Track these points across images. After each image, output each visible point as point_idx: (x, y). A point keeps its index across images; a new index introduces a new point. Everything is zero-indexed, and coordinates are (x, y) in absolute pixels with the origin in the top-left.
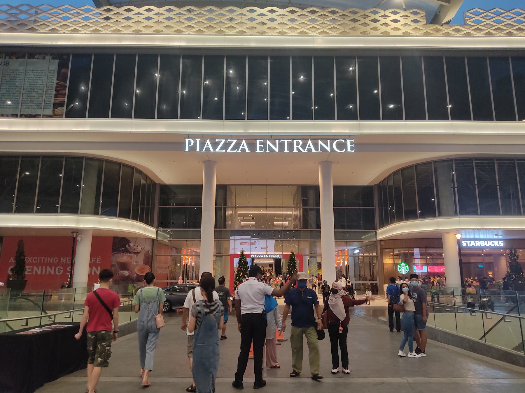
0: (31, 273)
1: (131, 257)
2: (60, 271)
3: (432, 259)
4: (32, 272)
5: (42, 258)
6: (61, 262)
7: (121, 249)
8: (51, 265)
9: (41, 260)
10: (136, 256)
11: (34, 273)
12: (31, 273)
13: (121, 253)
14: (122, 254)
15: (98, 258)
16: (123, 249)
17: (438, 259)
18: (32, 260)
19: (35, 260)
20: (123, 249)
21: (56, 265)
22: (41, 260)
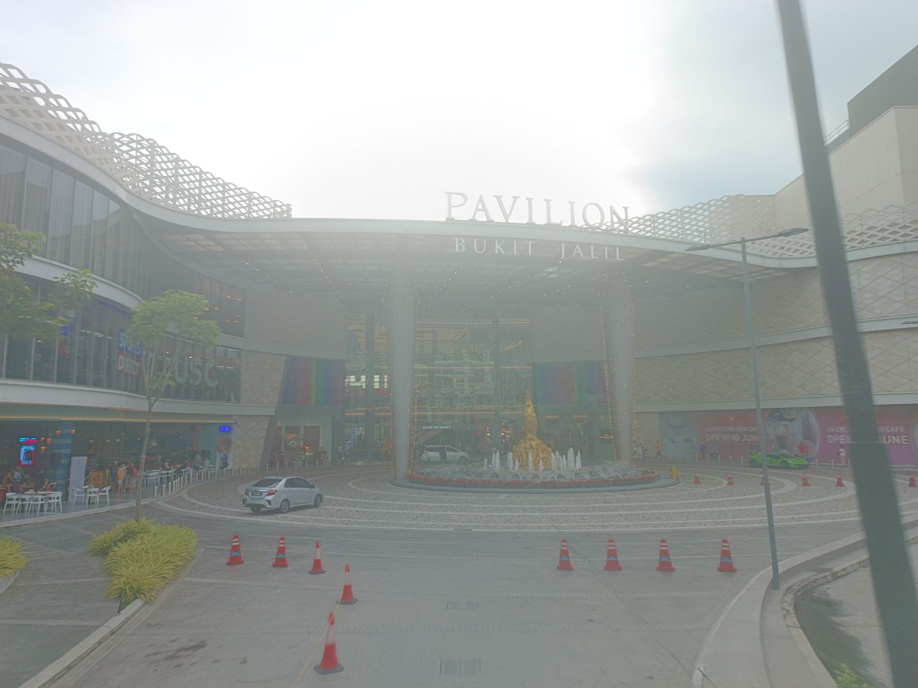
16: (778, 414)
20: (778, 414)
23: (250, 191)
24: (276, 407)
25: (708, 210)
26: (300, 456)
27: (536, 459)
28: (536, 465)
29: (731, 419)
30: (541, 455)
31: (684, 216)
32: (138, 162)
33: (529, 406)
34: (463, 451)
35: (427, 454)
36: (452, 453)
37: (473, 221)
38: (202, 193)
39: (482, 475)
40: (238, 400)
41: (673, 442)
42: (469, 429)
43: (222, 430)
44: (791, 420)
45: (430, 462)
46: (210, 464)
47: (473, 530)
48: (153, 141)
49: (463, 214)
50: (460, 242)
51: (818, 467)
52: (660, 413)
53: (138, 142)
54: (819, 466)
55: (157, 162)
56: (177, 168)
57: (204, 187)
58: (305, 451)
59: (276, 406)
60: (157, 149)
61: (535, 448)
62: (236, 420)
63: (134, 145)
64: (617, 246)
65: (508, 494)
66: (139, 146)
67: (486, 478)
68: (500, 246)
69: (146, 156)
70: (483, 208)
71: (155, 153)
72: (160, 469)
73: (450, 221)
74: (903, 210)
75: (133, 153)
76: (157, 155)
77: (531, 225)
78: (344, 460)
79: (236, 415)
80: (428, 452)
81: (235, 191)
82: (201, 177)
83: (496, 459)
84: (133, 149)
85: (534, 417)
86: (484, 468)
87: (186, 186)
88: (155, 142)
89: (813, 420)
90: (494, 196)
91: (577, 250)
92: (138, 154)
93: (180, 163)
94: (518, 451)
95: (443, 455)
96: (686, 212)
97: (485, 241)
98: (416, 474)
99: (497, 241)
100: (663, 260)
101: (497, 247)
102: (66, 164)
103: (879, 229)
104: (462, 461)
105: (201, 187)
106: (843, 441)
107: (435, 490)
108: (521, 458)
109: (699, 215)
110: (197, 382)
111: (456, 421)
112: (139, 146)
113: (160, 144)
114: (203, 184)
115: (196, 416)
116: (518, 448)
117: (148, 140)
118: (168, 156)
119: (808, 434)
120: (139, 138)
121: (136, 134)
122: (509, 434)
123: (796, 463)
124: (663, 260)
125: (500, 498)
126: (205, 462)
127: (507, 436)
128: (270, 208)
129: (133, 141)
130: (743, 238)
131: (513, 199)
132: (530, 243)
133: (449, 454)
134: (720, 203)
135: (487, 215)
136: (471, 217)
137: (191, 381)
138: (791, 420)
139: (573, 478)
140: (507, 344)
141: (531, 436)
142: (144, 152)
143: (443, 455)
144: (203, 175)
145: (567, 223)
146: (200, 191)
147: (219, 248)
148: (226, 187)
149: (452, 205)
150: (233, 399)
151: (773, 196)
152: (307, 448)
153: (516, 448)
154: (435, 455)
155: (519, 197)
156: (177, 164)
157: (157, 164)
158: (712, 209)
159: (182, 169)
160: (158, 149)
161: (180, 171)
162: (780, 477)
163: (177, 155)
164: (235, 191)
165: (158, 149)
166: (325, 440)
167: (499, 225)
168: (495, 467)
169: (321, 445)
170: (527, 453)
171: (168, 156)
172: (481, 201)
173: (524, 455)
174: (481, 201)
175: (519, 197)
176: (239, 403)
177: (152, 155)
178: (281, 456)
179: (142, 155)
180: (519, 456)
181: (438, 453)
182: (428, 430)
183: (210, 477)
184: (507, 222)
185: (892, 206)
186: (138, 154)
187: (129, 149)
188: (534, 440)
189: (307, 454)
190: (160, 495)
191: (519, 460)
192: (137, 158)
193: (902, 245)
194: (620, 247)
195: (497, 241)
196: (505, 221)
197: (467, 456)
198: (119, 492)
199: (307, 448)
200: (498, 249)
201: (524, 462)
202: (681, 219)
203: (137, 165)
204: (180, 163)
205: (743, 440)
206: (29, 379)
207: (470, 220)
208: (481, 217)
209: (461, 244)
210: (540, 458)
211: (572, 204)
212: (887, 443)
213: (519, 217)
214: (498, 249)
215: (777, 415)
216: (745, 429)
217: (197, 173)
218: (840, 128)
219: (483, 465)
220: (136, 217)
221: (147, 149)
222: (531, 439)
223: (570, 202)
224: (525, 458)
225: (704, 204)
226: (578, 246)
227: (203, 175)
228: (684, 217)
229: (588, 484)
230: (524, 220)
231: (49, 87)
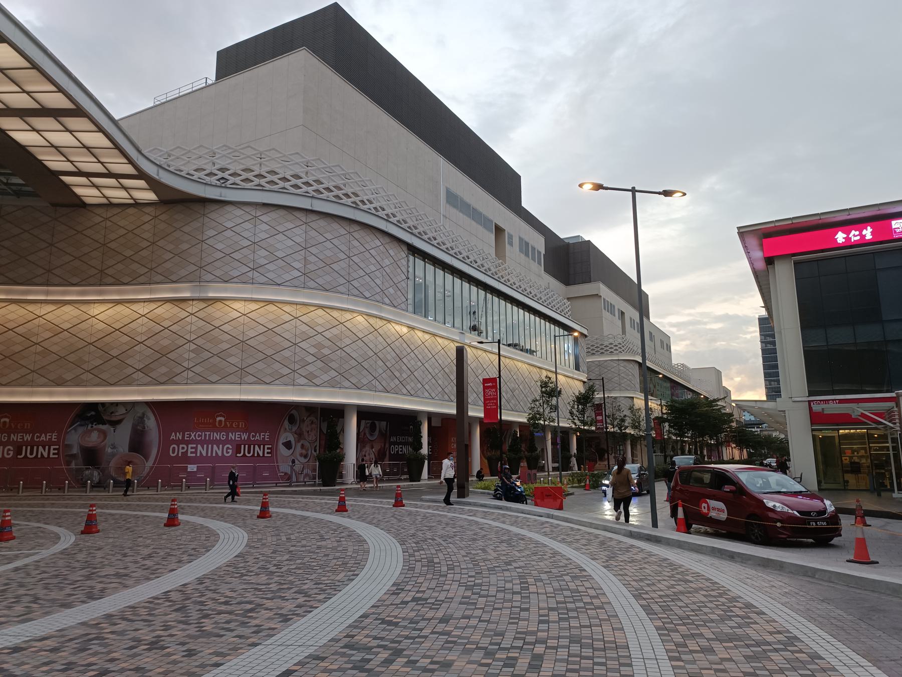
0: (194, 455)
1: (104, 434)
2: (228, 451)
3: (483, 370)
4: (196, 452)
5: (208, 433)
6: (11, 440)
7: (89, 415)
8: (218, 442)
9: (205, 435)
10: (113, 431)
11: (198, 455)
12: (194, 455)
13: (88, 425)
14: (90, 425)
15: (54, 434)
16: (93, 413)
17: (391, 222)
18: (195, 436)
19: (199, 436)
20: (93, 413)
21: (224, 443)
22: (205, 435)
29: (218, 419)
74: (261, 155)
89: (151, 422)
103: (280, 176)
119: (138, 445)
130: (634, 188)
138: (115, 423)
162: (194, 515)
185: (273, 149)
193: (309, 200)
216: (28, 437)
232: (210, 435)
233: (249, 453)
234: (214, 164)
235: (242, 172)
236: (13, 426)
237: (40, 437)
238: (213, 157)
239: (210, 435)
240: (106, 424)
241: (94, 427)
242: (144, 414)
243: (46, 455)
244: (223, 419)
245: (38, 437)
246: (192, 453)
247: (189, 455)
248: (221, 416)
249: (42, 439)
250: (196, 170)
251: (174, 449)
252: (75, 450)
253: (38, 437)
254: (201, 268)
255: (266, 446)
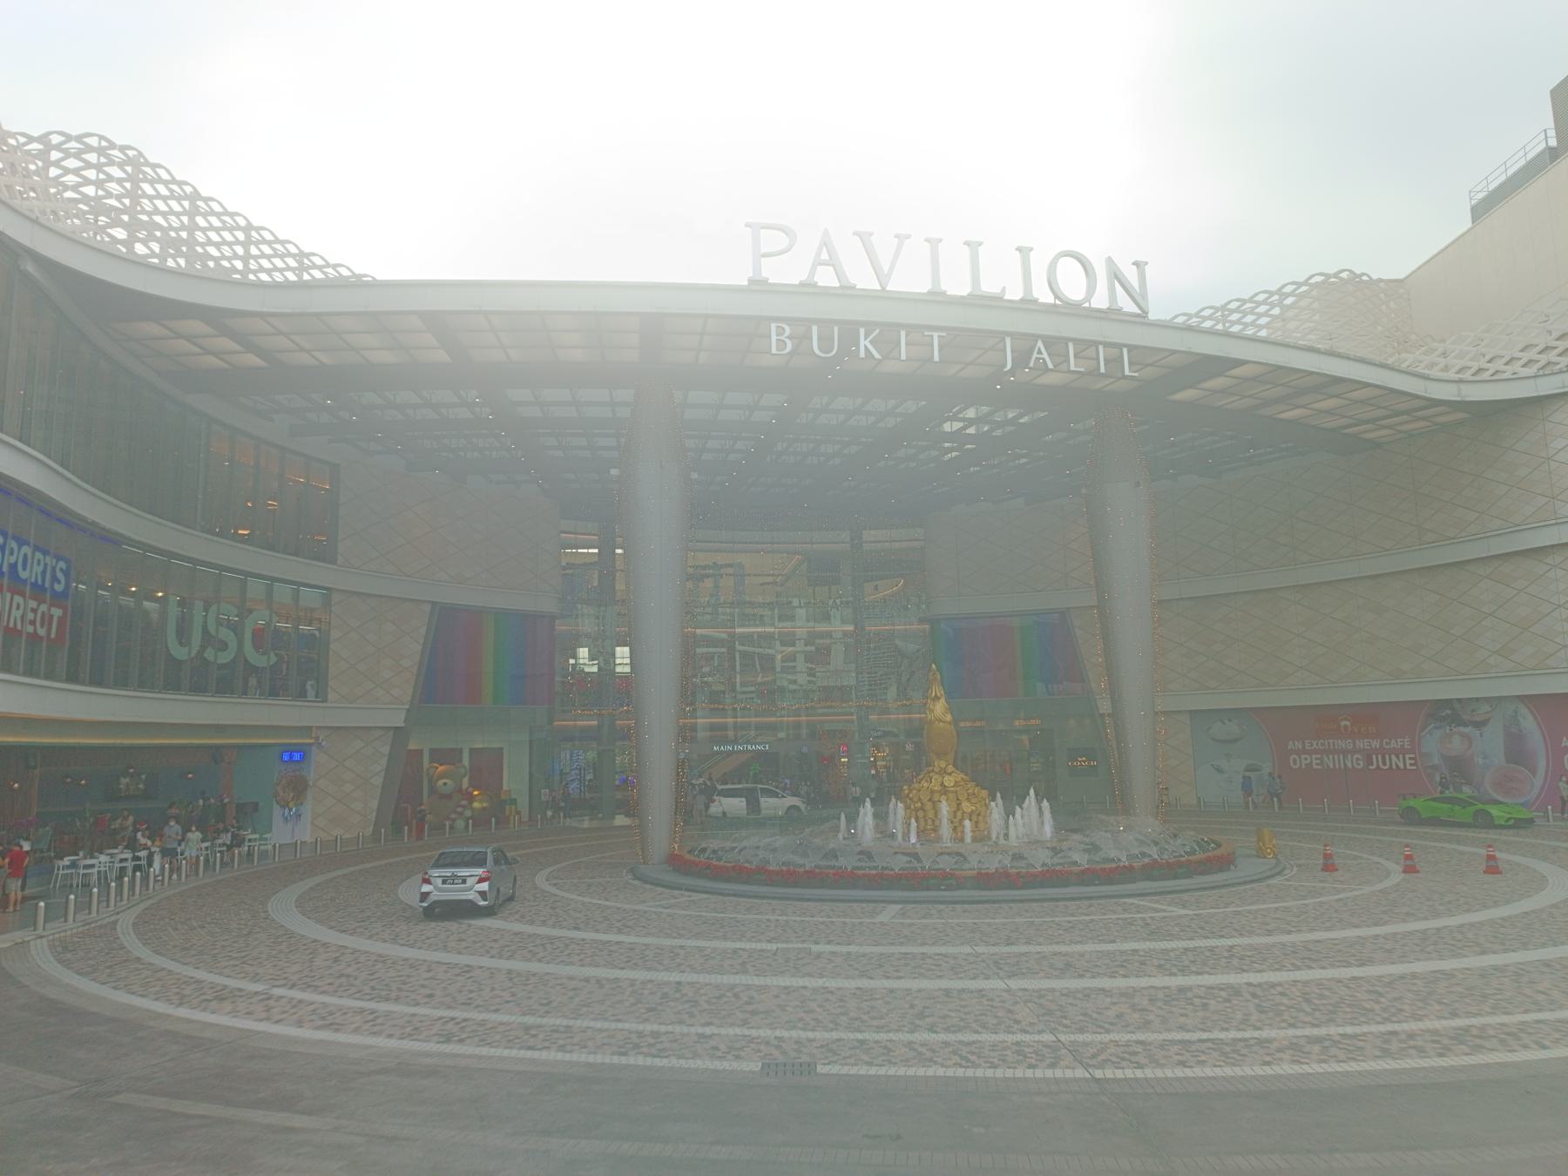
8: (1345, 752)
18: (1317, 744)
20: (1449, 712)
23: (357, 272)
24: (408, 710)
25: (1280, 303)
26: (459, 810)
27: (955, 817)
28: (957, 828)
29: (1343, 723)
30: (967, 807)
31: (1230, 318)
32: (101, 193)
33: (937, 698)
34: (794, 795)
35: (720, 802)
36: (772, 801)
37: (808, 289)
38: (249, 269)
39: (836, 857)
40: (321, 695)
41: (1220, 770)
42: (805, 750)
43: (286, 758)
44: (1480, 725)
45: (728, 822)
46: (203, 841)
47: (821, 1069)
48: (135, 153)
49: (786, 271)
50: (780, 331)
51: (1552, 823)
52: (1191, 711)
53: (100, 151)
54: (1554, 821)
55: (145, 195)
56: (193, 213)
57: (255, 258)
58: (471, 798)
59: (407, 707)
60: (143, 168)
61: (952, 792)
62: (317, 738)
63: (92, 157)
64: (1125, 346)
65: (900, 906)
66: (103, 160)
67: (847, 862)
68: (871, 342)
69: (120, 181)
70: (831, 259)
71: (141, 176)
72: (81, 854)
73: (758, 286)
75: (91, 174)
76: (145, 180)
77: (937, 298)
78: (553, 817)
79: (318, 728)
80: (722, 798)
81: (325, 270)
82: (248, 236)
83: (867, 812)
84: (89, 165)
85: (949, 723)
86: (840, 836)
87: (212, 251)
88: (141, 154)
90: (855, 233)
91: (1040, 352)
92: (102, 176)
93: (200, 203)
94: (915, 800)
95: (754, 805)
96: (1232, 311)
97: (836, 329)
98: (689, 852)
99: (862, 331)
100: (1218, 383)
101: (863, 342)
102: (38, 253)
104: (791, 819)
105: (245, 259)
106: (1317, 764)
107: (729, 895)
108: (921, 814)
109: (1260, 315)
110: (224, 658)
111: (782, 735)
112: (103, 160)
113: (152, 160)
114: (254, 251)
115: (220, 729)
116: (914, 792)
117: (123, 149)
118: (170, 186)
119: (1516, 751)
120: (104, 143)
121: (98, 135)
122: (883, 758)
123: (1508, 816)
124: (1218, 383)
125: (879, 919)
126: (190, 835)
127: (878, 763)
128: (260, 257)
129: (90, 149)
131: (897, 240)
132: (935, 335)
133: (767, 803)
134: (1304, 288)
135: (839, 274)
136: (803, 277)
137: (209, 654)
138: (1480, 725)
139: (1048, 861)
140: (876, 587)
141: (943, 764)
142: (115, 172)
143: (754, 805)
144: (254, 233)
145: (1015, 293)
146: (246, 264)
147: (252, 360)
148: (306, 261)
149: (763, 251)
150: (311, 693)
151: (1401, 281)
152: (476, 793)
153: (910, 791)
154: (736, 805)
155: (909, 237)
156: (193, 204)
157: (145, 201)
158: (1289, 301)
159: (205, 215)
160: (148, 170)
161: (200, 221)
163: (192, 186)
164: (325, 270)
165: (148, 170)
166: (514, 780)
167: (867, 295)
168: (863, 833)
169: (505, 787)
170: (935, 804)
171: (170, 186)
172: (826, 243)
173: (929, 806)
174: (826, 243)
175: (909, 237)
176: (325, 701)
177: (134, 180)
178: (421, 811)
179: (110, 178)
180: (917, 810)
181: (743, 799)
182: (729, 754)
183: (239, 865)
184: (883, 289)
186: (102, 176)
187: (81, 164)
188: (950, 774)
189: (476, 805)
190: (105, 904)
191: (917, 821)
192: (99, 184)
194: (1131, 348)
195: (862, 331)
196: (879, 288)
197: (802, 807)
198: (11, 909)
199: (476, 793)
200: (866, 347)
201: (930, 822)
202: (1224, 325)
203: (97, 198)
204: (200, 203)
205: (1371, 767)
206: (232, 692)
207: (802, 284)
208: (826, 278)
209: (782, 338)
210: (964, 812)
211: (1024, 252)
212: (1294, 767)
213: (911, 279)
214: (866, 347)
215: (1448, 713)
216: (1376, 744)
217: (239, 228)
218: (1490, 179)
219: (836, 829)
220: (30, 268)
221: (121, 166)
222: (943, 772)
223: (1019, 249)
224: (931, 814)
225: (1271, 294)
226: (1040, 344)
227: (254, 233)
228: (1230, 321)
229: (1088, 876)
230: (922, 286)
231: (27, 132)
232: (1334, 743)
233: (1384, 764)
234: (1550, 332)
235: (1489, 364)
236: (1356, 731)
237: (1390, 743)
238: (1546, 321)
239: (1334, 743)
240: (1468, 726)
241: (1455, 730)
242: (1516, 712)
243: (1401, 766)
244: (1348, 723)
245: (1387, 743)
246: (1317, 764)
247: (1315, 767)
248: (1345, 719)
249: (1392, 746)
250: (1522, 351)
251: (1295, 760)
252: (1436, 761)
253: (1387, 743)
254: (1554, 498)
255: (1407, 756)
